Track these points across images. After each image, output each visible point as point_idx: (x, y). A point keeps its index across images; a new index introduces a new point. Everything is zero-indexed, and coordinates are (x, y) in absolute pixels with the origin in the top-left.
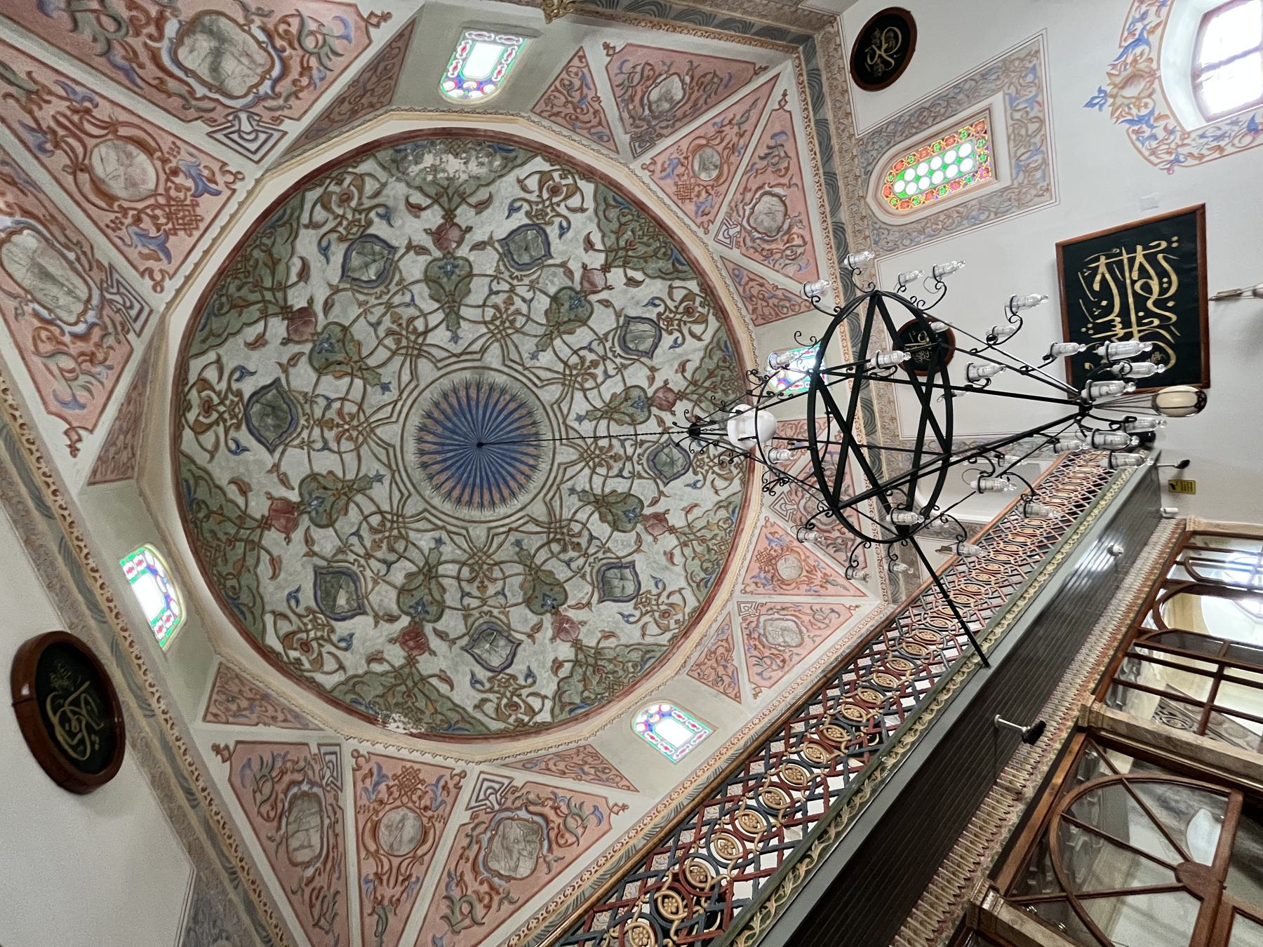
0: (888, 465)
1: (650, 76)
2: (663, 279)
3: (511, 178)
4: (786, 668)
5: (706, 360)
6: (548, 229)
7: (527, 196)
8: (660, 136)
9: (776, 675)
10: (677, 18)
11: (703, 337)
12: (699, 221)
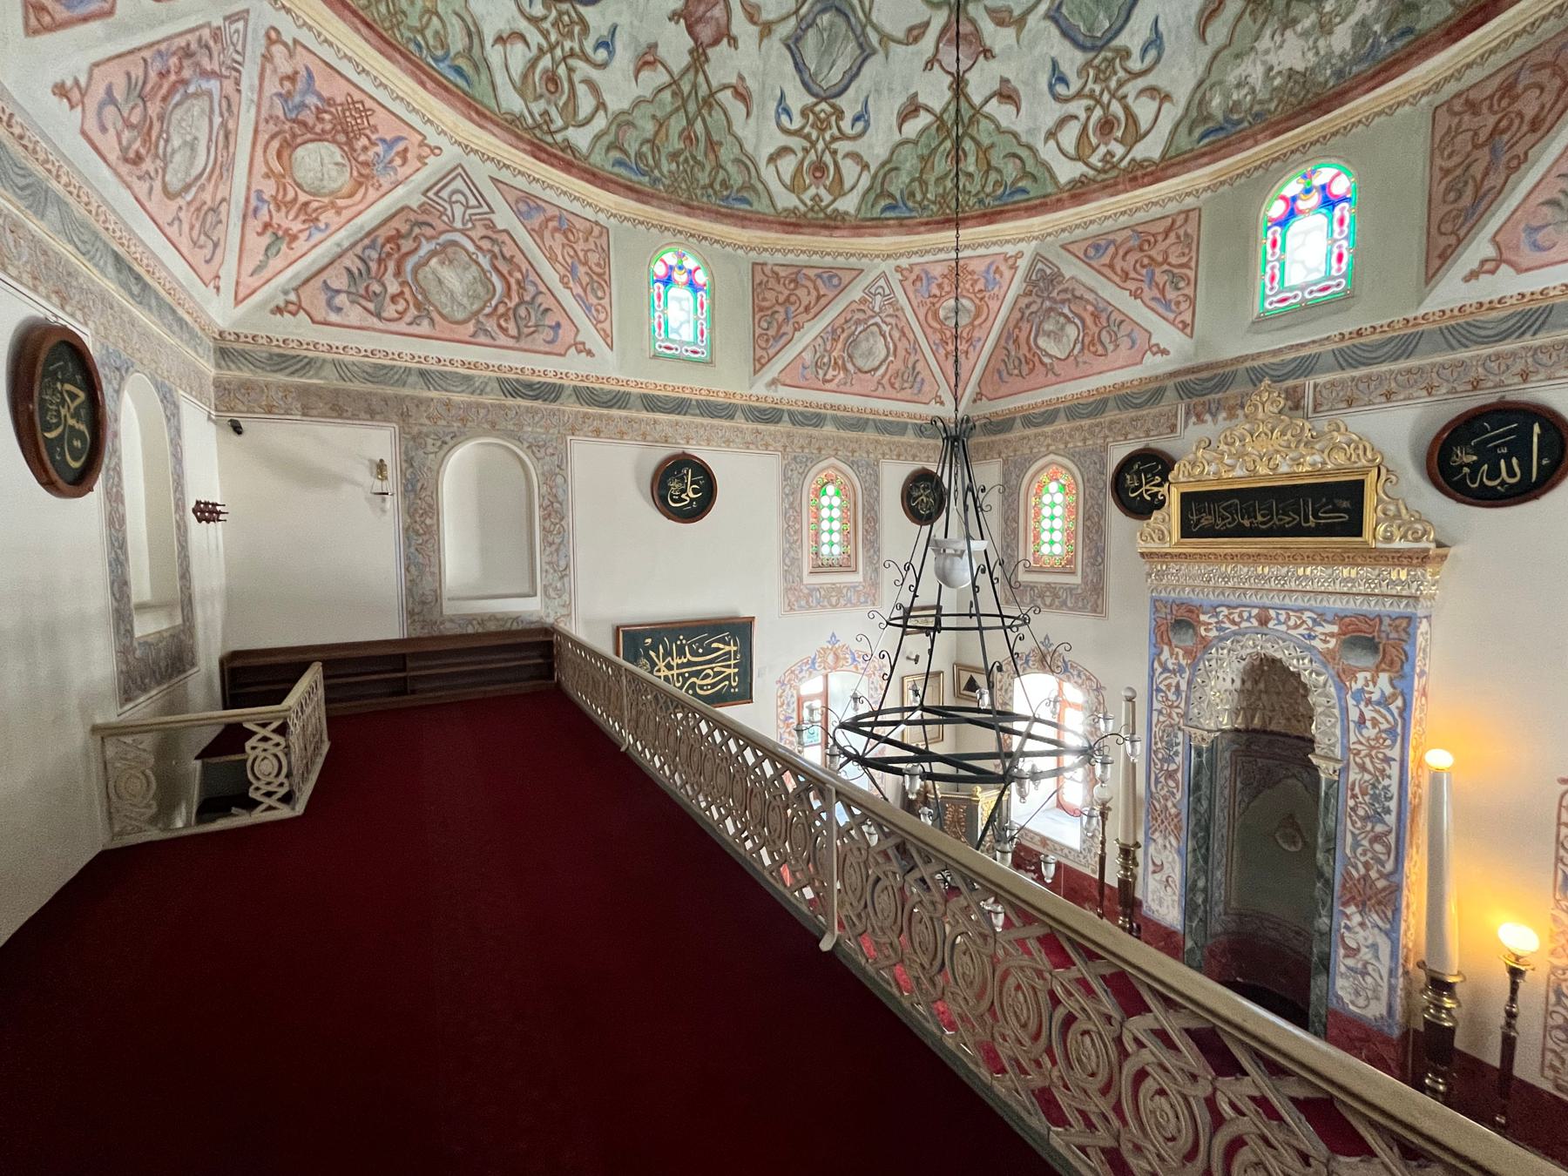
0: (528, 410)
1: (1092, 345)
2: (883, 165)
3: (1182, 94)
4: (124, 169)
5: (737, 150)
6: (1080, 57)
7: (1141, 83)
8: (1027, 294)
9: (109, 143)
10: (1105, 402)
11: (772, 168)
12: (917, 270)
